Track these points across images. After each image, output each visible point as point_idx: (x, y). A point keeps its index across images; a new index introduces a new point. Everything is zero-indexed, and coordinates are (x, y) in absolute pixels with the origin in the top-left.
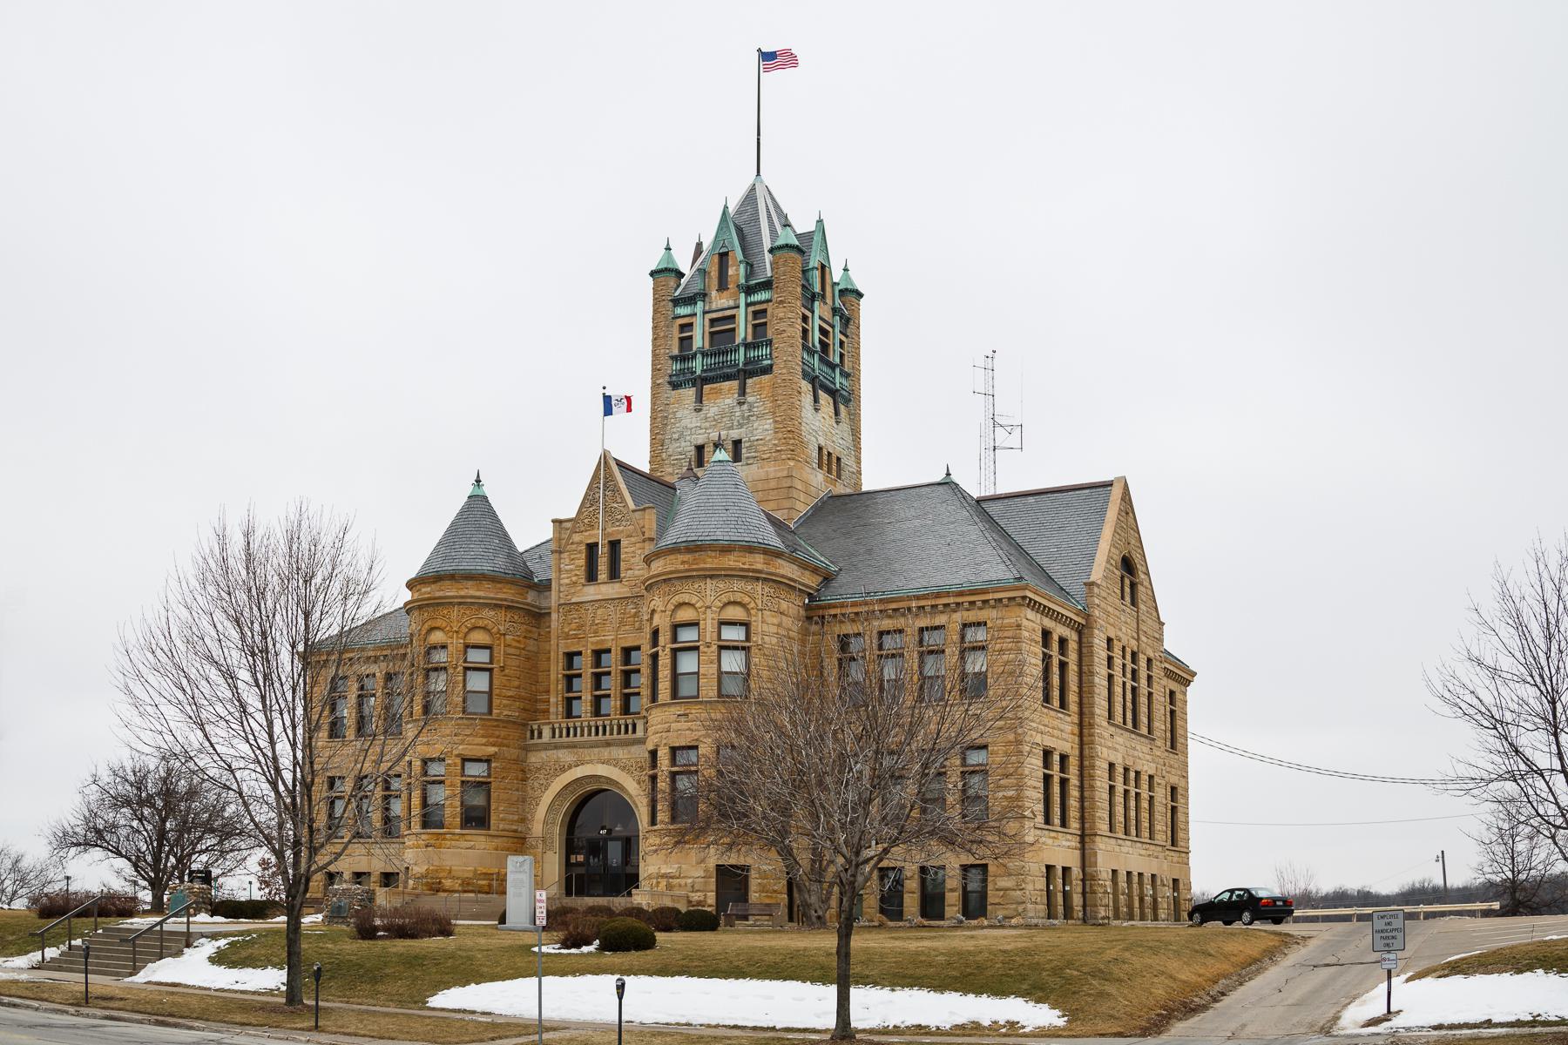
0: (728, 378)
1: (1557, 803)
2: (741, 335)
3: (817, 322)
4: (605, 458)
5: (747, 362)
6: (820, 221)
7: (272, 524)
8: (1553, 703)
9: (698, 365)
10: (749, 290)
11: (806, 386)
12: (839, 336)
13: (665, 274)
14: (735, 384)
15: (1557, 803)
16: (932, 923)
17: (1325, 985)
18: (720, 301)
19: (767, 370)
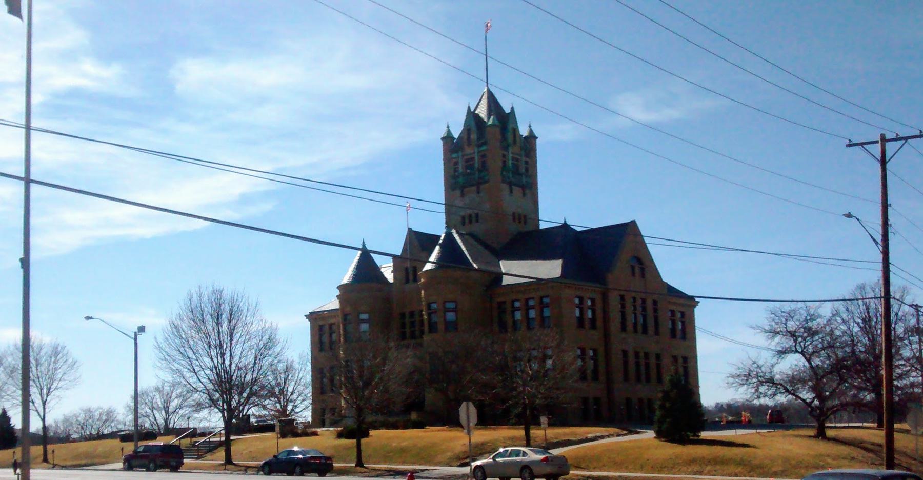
0: (473, 185)
1: (44, 420)
2: (476, 165)
3: (511, 155)
4: (410, 230)
5: (480, 178)
6: (512, 108)
7: (106, 407)
8: (778, 333)
9: (461, 180)
10: (479, 146)
11: (505, 187)
12: (524, 159)
13: (448, 139)
14: (474, 188)
15: (44, 420)
16: (865, 424)
17: (39, 414)
18: (469, 151)
19: (487, 182)
